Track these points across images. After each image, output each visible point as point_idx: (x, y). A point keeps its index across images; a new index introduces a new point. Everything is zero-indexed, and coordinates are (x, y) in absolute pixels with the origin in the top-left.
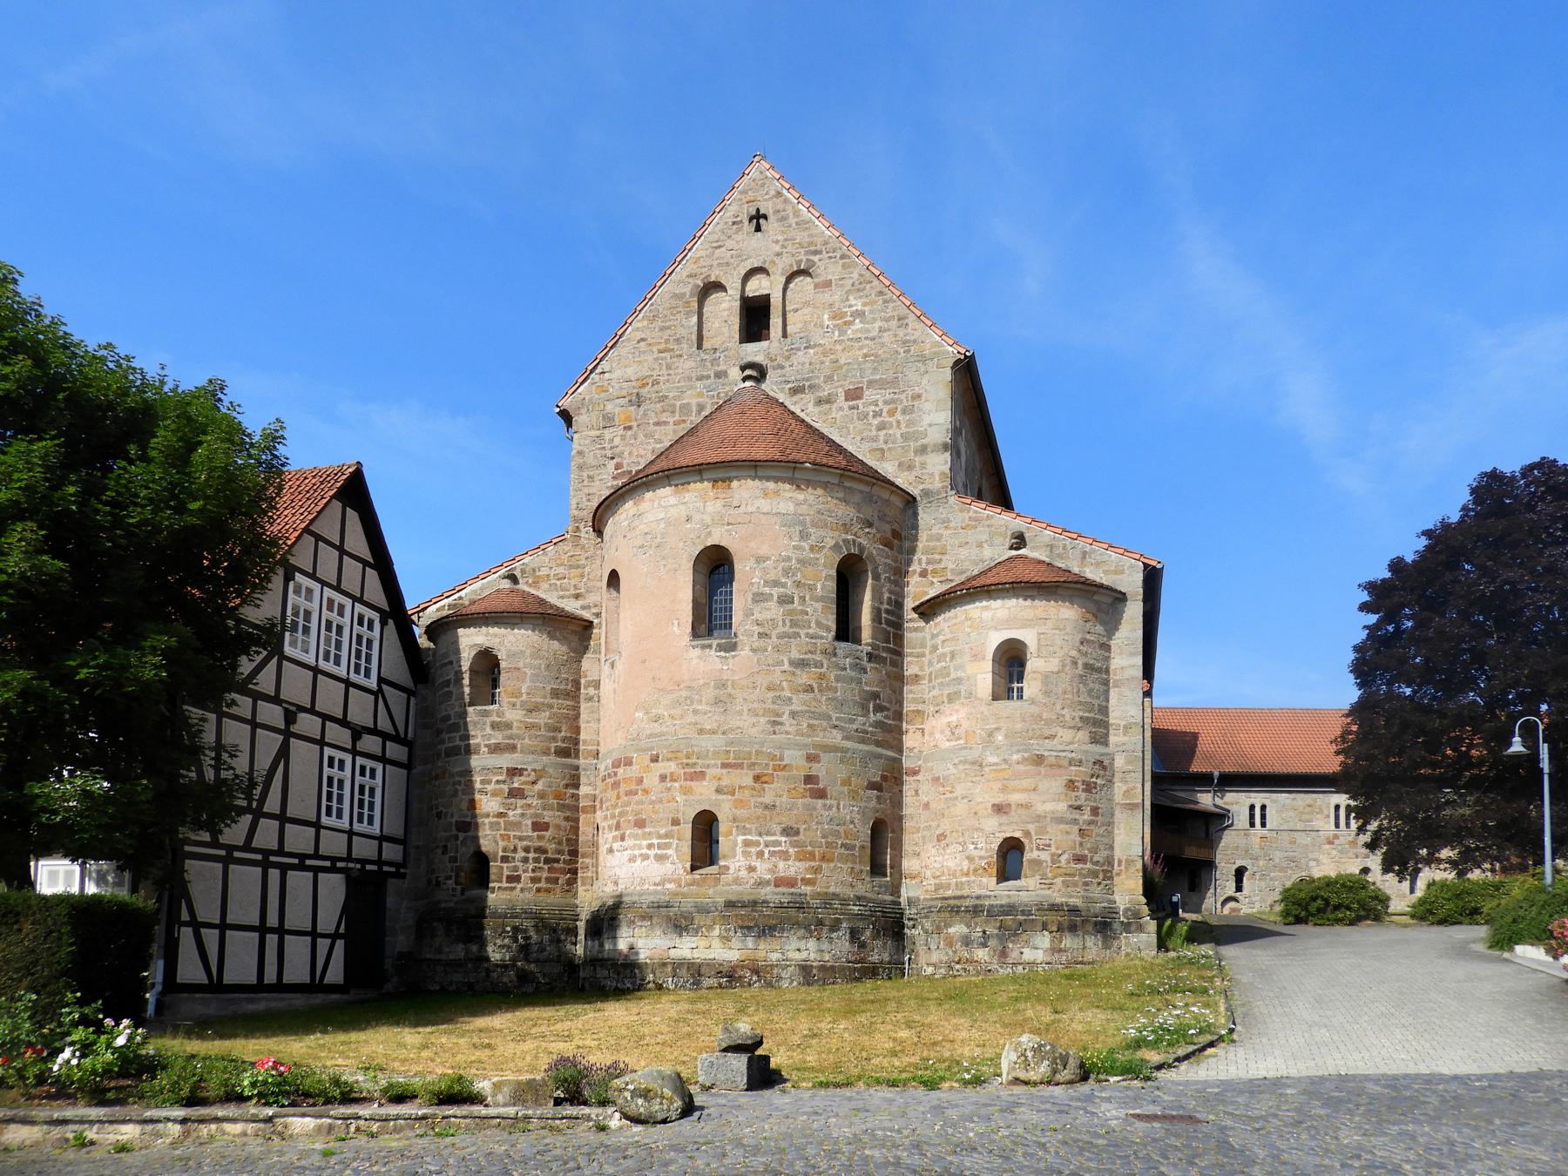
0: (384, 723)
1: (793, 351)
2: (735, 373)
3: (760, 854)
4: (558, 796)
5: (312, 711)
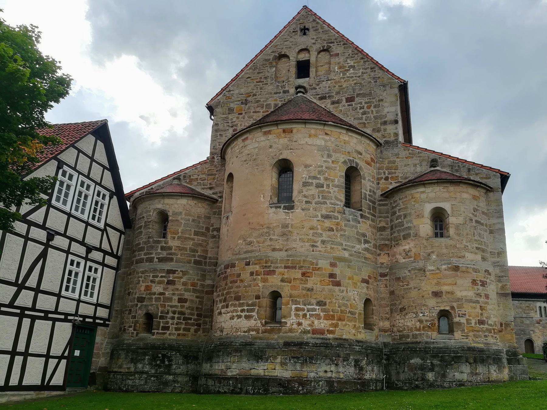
0: (105, 246)
1: (320, 82)
2: (292, 91)
3: (305, 316)
4: (193, 285)
5: (64, 235)
